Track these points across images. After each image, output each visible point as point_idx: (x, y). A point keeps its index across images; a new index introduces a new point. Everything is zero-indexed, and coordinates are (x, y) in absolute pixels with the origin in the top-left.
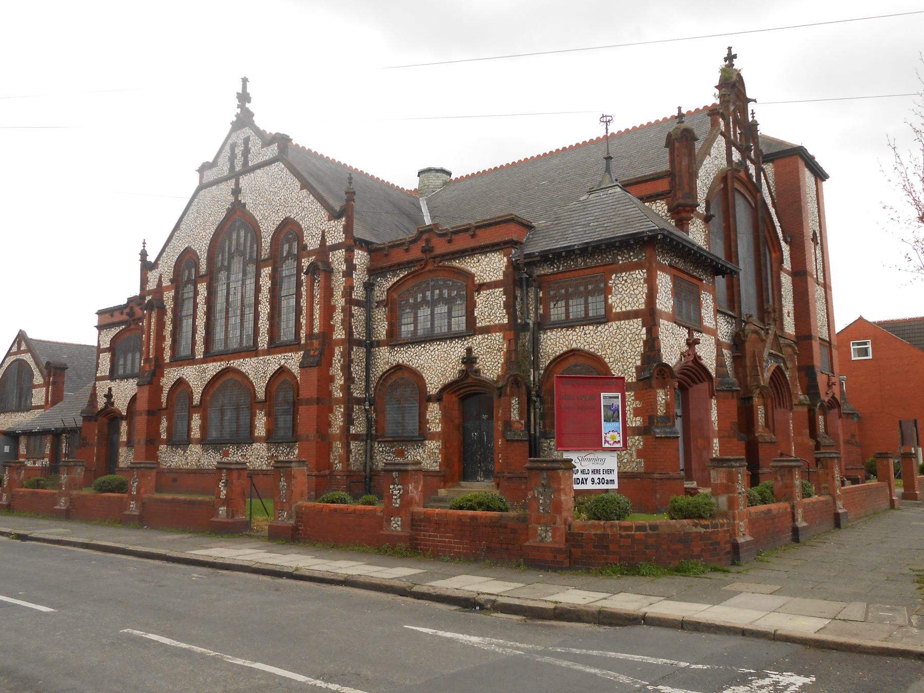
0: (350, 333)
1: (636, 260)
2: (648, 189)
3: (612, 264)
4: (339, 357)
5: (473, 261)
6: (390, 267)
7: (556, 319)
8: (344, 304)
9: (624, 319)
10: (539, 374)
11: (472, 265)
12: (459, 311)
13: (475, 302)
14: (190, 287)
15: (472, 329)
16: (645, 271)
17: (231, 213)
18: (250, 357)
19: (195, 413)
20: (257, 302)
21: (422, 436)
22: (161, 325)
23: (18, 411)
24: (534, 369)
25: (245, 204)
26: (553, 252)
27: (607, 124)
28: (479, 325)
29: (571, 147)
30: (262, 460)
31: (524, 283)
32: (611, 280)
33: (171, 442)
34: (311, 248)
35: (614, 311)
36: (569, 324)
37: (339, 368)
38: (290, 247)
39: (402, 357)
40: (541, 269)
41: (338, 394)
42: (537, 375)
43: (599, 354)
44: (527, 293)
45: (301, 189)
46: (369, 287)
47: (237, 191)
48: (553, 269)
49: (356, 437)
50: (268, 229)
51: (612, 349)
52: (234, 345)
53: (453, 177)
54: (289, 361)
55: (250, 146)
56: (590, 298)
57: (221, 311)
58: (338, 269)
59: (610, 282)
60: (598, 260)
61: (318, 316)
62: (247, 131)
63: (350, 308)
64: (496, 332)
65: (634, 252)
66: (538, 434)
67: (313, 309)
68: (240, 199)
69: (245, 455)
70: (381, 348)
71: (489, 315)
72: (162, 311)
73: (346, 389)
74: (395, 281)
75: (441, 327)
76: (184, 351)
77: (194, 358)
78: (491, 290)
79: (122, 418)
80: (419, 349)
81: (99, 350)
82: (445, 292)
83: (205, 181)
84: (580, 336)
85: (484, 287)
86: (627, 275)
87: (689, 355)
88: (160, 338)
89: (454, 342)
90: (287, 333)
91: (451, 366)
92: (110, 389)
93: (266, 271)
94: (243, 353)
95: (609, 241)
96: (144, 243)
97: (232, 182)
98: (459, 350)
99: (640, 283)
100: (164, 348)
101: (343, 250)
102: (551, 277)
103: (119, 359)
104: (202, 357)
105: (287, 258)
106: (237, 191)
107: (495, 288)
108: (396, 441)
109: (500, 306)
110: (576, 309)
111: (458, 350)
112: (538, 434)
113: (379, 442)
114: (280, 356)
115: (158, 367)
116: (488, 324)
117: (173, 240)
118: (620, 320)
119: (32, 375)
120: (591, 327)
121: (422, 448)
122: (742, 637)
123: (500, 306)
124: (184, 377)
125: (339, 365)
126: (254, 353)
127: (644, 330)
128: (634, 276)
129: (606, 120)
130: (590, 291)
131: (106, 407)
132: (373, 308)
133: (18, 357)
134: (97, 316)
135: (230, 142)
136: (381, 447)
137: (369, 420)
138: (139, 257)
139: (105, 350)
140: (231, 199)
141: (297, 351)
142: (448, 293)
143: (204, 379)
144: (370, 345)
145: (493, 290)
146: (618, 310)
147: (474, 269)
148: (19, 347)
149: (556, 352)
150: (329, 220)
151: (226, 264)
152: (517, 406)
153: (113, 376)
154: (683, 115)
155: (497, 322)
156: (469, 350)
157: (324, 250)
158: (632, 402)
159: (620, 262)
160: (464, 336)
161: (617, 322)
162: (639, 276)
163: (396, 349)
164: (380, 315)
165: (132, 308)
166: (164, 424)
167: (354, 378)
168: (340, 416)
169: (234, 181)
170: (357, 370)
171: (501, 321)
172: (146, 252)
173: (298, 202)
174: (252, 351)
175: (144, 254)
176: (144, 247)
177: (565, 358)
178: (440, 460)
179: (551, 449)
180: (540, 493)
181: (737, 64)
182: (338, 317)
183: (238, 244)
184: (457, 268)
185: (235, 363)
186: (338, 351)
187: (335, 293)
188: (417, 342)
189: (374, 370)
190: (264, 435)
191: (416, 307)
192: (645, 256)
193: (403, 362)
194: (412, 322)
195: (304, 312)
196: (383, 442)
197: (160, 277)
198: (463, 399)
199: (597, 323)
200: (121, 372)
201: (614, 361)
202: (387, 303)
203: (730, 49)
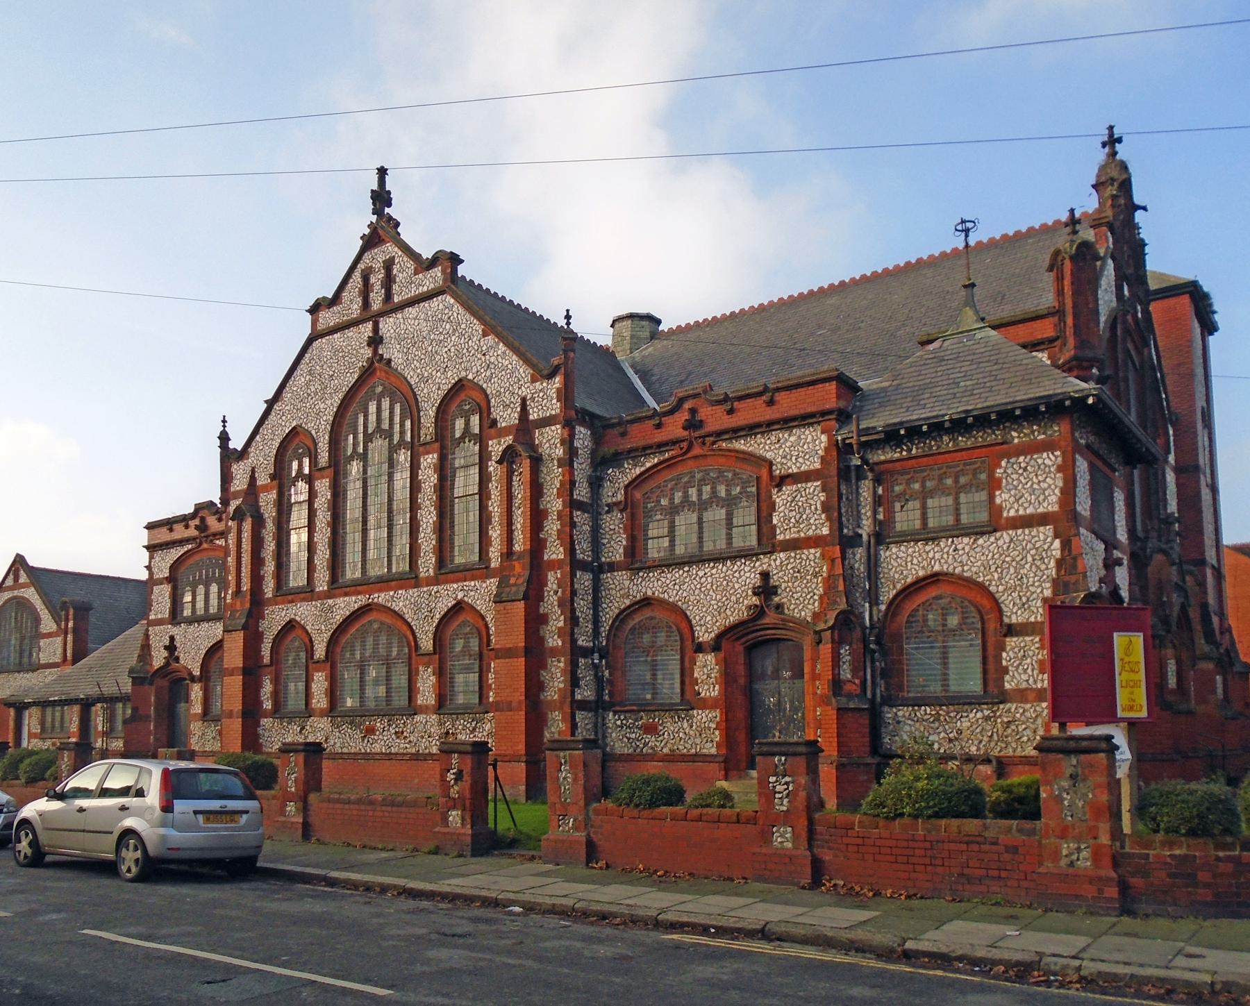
0: (571, 551)
1: (1043, 436)
2: (1023, 332)
3: (1002, 444)
4: (555, 587)
5: (768, 442)
6: (630, 451)
7: (905, 528)
8: (560, 508)
9: (1023, 527)
10: (879, 611)
11: (767, 448)
12: (746, 515)
13: (774, 503)
14: (302, 486)
15: (768, 543)
16: (1058, 453)
17: (367, 373)
18: (406, 588)
19: (318, 671)
20: (414, 506)
21: (689, 702)
23: (19, 672)
24: (870, 603)
25: (389, 361)
26: (906, 425)
27: (967, 236)
28: (780, 537)
29: (853, 280)
30: (431, 739)
31: (853, 474)
32: (1000, 467)
33: (278, 710)
34: (503, 425)
35: (1005, 514)
36: (927, 535)
37: (556, 603)
38: (467, 423)
39: (651, 586)
40: (880, 452)
42: (875, 612)
43: (981, 579)
44: (857, 489)
45: (485, 334)
46: (596, 484)
47: (375, 341)
48: (901, 452)
49: (583, 705)
50: (430, 398)
51: (1002, 573)
52: (377, 570)
53: (663, 327)
54: (472, 593)
55: (395, 272)
56: (962, 496)
57: (354, 521)
58: (549, 455)
59: (998, 471)
60: (980, 438)
61: (519, 526)
62: (390, 249)
63: (571, 513)
64: (809, 547)
65: (1039, 425)
66: (878, 699)
67: (512, 516)
68: (380, 352)
69: (402, 732)
70: (616, 574)
71: (797, 522)
72: (259, 522)
74: (638, 472)
75: (715, 542)
76: (297, 578)
78: (799, 485)
79: (193, 679)
80: (677, 574)
81: (151, 582)
82: (693, 492)
83: (320, 327)
84: (948, 553)
85: (788, 480)
86: (1027, 460)
88: (257, 562)
89: (738, 563)
90: (465, 552)
91: (733, 598)
92: (172, 638)
93: (429, 460)
94: (393, 583)
95: (1003, 408)
96: (224, 421)
97: (366, 327)
98: (748, 575)
99: (1050, 472)
100: (264, 576)
101: (558, 426)
102: (897, 464)
103: (183, 595)
104: (326, 588)
106: (375, 341)
107: (807, 481)
108: (644, 711)
109: (816, 509)
110: (939, 510)
111: (747, 575)
112: (878, 699)
113: (615, 713)
114: (455, 586)
116: (797, 536)
117: (271, 417)
118: (1015, 527)
119: (37, 620)
120: (966, 540)
121: (688, 721)
123: (816, 509)
124: (298, 618)
125: (555, 598)
126: (413, 581)
127: (1057, 543)
128: (1040, 461)
129: (965, 228)
130: (964, 486)
131: (167, 664)
132: (600, 514)
133: (16, 593)
134: (146, 531)
135: (361, 266)
136: (619, 719)
137: (599, 680)
138: (218, 442)
139: (160, 582)
140: (368, 352)
141: (484, 578)
142: (727, 490)
143: (331, 621)
144: (598, 569)
145: (804, 485)
146: (1012, 513)
147: (770, 453)
148: (16, 579)
149: (906, 577)
150: (534, 380)
151: (361, 450)
152: (848, 658)
154: (1078, 222)
155: (810, 533)
156: (765, 576)
157: (525, 427)
158: (1037, 651)
159: (1016, 441)
160: (757, 555)
161: (1010, 532)
162: (1047, 462)
163: (641, 574)
164: (613, 523)
165: (203, 519)
167: (578, 617)
168: (559, 675)
169: (370, 325)
170: (583, 606)
171: (818, 531)
172: (227, 434)
173: (479, 356)
174: (411, 579)
175: (224, 438)
176: (224, 426)
177: (922, 586)
178: (718, 739)
179: (899, 722)
180: (1065, 790)
181: (1123, 151)
183: (379, 419)
184: (743, 452)
185: (381, 598)
187: (545, 491)
188: (676, 564)
189: (604, 606)
190: (433, 702)
191: (673, 510)
192: (1059, 431)
193: (653, 593)
194: (666, 534)
195: (496, 519)
196: (622, 712)
197: (253, 471)
198: (751, 649)
199: (976, 534)
200: (187, 612)
201: (1005, 590)
202: (627, 506)
203: (1111, 128)
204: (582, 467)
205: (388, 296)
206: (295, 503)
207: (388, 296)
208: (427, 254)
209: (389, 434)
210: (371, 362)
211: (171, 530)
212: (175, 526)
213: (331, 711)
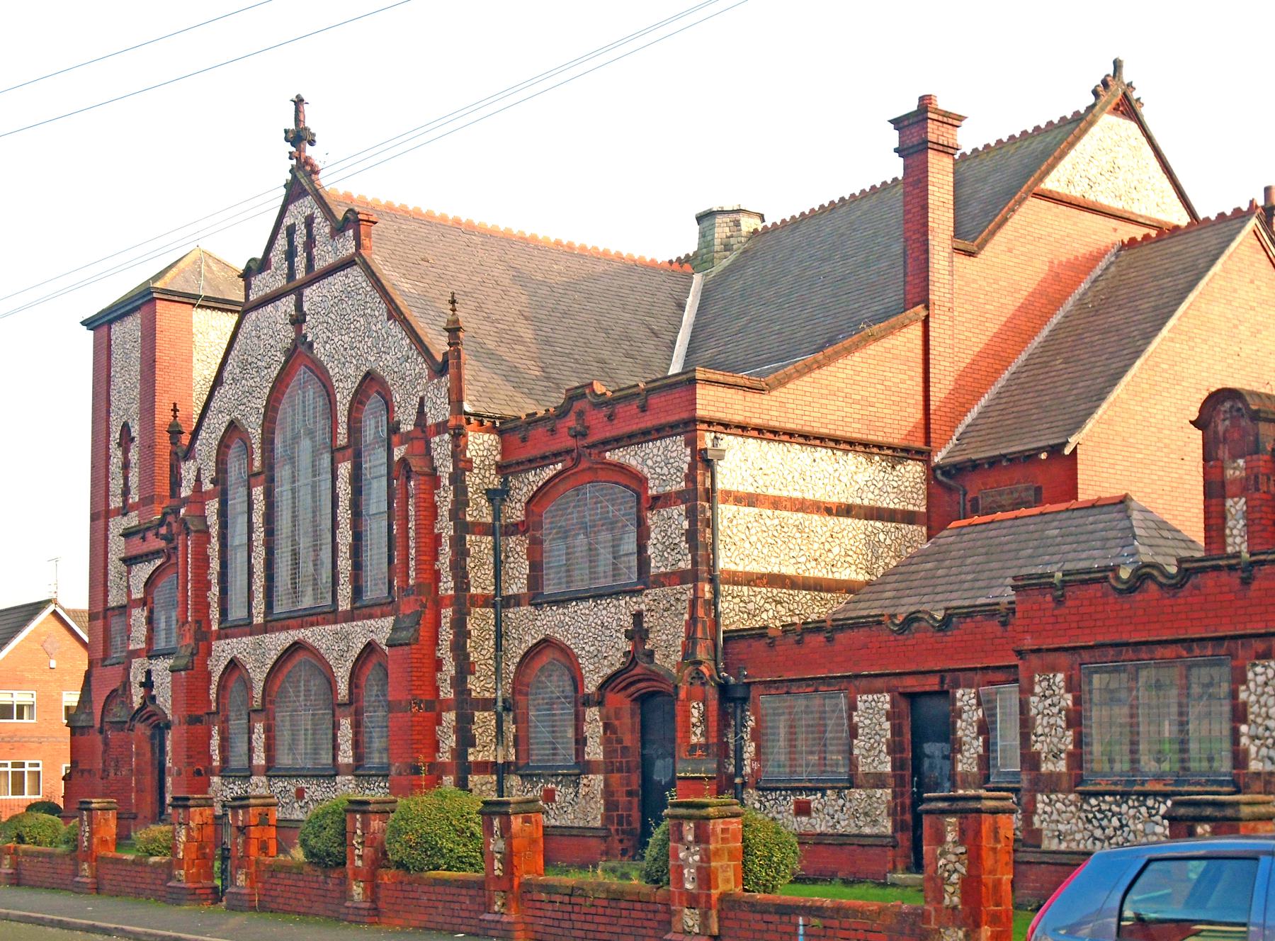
15: (645, 579)
41: (447, 692)
46: (496, 497)
47: (298, 320)
62: (306, 206)
73: (459, 682)
76: (237, 612)
87: (238, 710)
92: (149, 673)
106: (298, 320)
111: (619, 613)
115: (203, 639)
122: (97, 896)
126: (330, 617)
131: (144, 706)
144: (501, 603)
153: (152, 654)
174: (331, 615)
186: (447, 613)
191: (565, 534)
210: (295, 342)
212: (620, 408)
213: (357, 767)
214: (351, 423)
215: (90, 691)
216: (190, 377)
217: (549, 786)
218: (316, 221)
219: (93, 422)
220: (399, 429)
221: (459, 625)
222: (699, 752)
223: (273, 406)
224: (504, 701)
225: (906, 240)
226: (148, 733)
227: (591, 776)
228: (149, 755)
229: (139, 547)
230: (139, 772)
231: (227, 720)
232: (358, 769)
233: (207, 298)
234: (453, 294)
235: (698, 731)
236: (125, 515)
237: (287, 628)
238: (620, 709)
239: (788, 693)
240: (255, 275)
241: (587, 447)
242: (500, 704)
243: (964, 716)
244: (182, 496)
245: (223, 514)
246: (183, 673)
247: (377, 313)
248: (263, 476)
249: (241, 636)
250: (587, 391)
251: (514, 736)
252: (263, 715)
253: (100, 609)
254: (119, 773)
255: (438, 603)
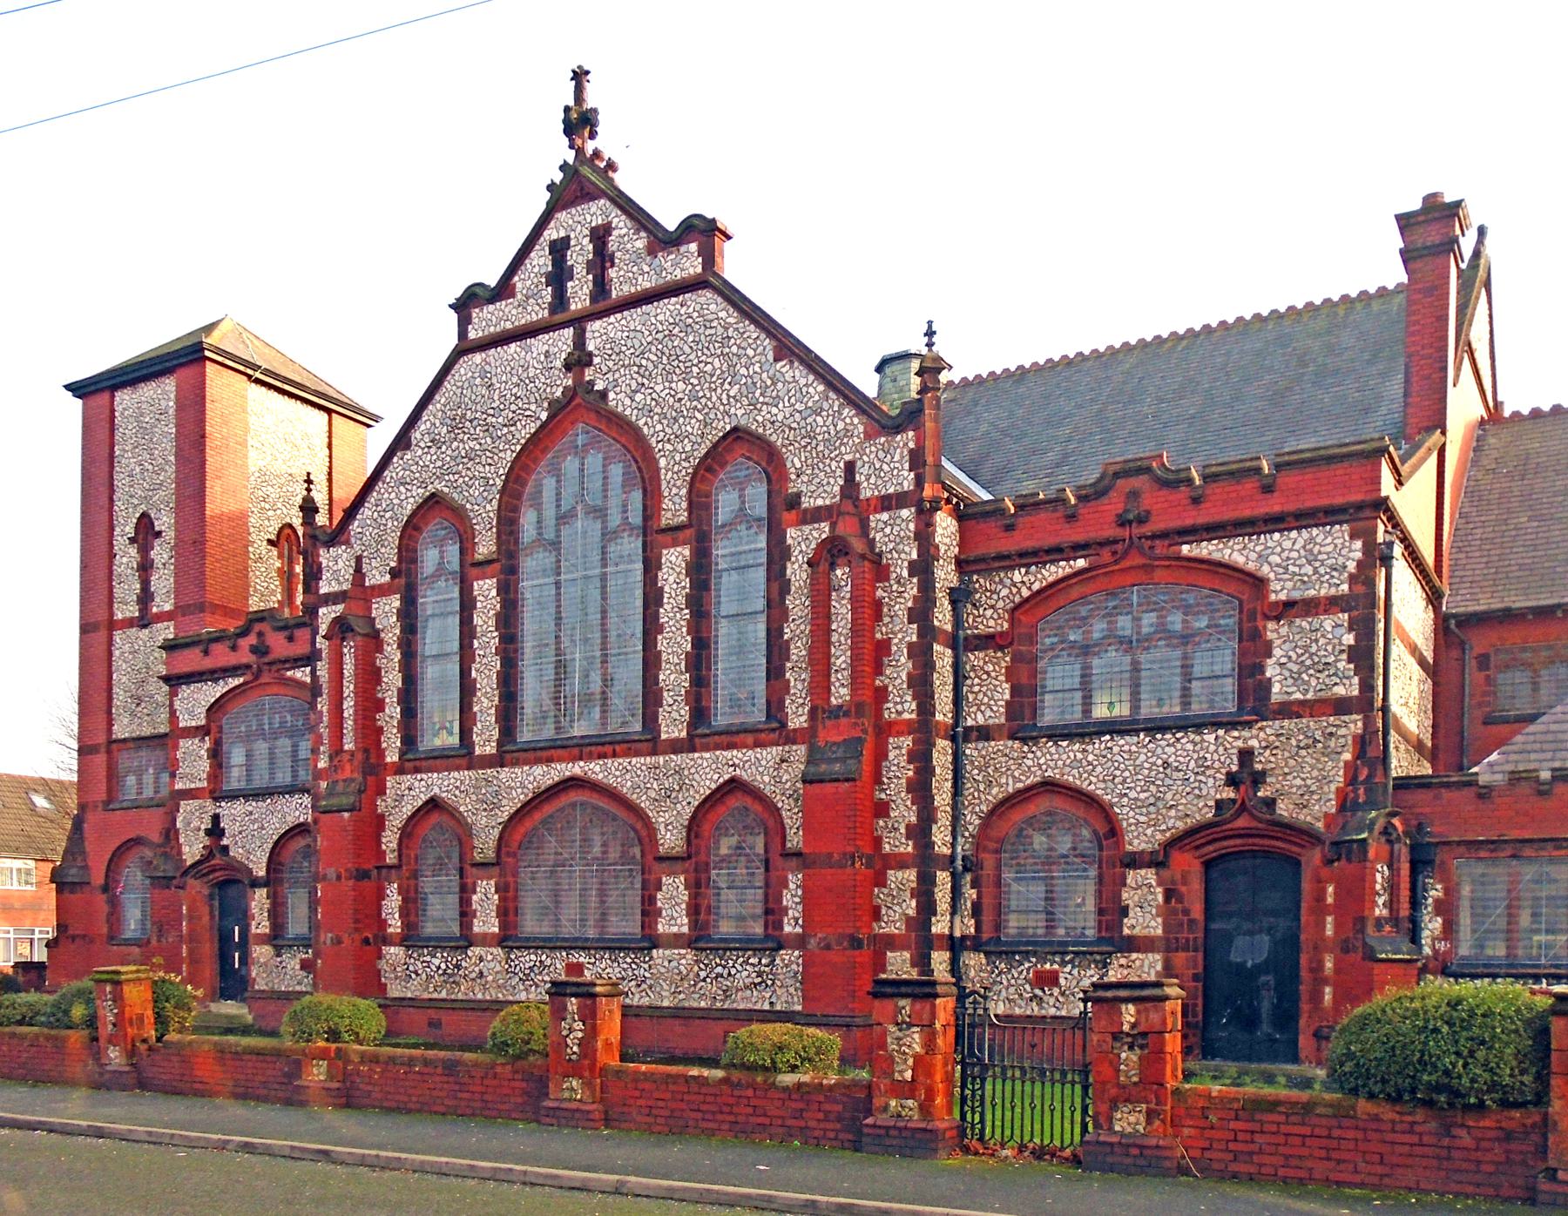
12: (1219, 659)
17: (562, 412)
22: (370, 676)
33: (411, 938)
46: (958, 597)
47: (579, 360)
62: (596, 212)
77: (655, 739)
79: (255, 883)
88: (370, 705)
93: (675, 559)
105: (436, 576)
106: (579, 360)
111: (1220, 748)
115: (373, 770)
131: (209, 854)
135: (551, 234)
153: (217, 792)
156: (1246, 755)
166: (392, 902)
174: (650, 742)
176: (309, 490)
182: (899, 669)
185: (595, 769)
191: (1086, 650)
204: (945, 575)
205: (601, 287)
206: (433, 615)
207: (601, 287)
208: (671, 223)
209: (600, 513)
210: (570, 393)
211: (206, 652)
214: (693, 495)
215: (82, 839)
216: (245, 466)
217: (1048, 966)
218: (615, 233)
219: (83, 512)
220: (799, 504)
221: (921, 758)
222: (1388, 928)
223: (518, 476)
224: (964, 859)
225: (1409, 356)
226: (206, 892)
227: (1134, 956)
228: (206, 919)
229: (192, 660)
230: (192, 938)
231: (415, 875)
232: (699, 939)
233: (267, 372)
234: (309, 474)
235: (1380, 901)
236: (145, 626)
237: (549, 760)
238: (1189, 872)
239: (1514, 856)
240: (480, 305)
241: (1147, 538)
242: (959, 862)
243: (664, 913)
244: (322, 591)
245: (409, 617)
246: (346, 815)
247: (750, 352)
248: (497, 566)
249: (449, 769)
250: (1154, 464)
251: (973, 904)
252: (496, 870)
253: (101, 739)
254: (163, 940)
255: (885, 730)
